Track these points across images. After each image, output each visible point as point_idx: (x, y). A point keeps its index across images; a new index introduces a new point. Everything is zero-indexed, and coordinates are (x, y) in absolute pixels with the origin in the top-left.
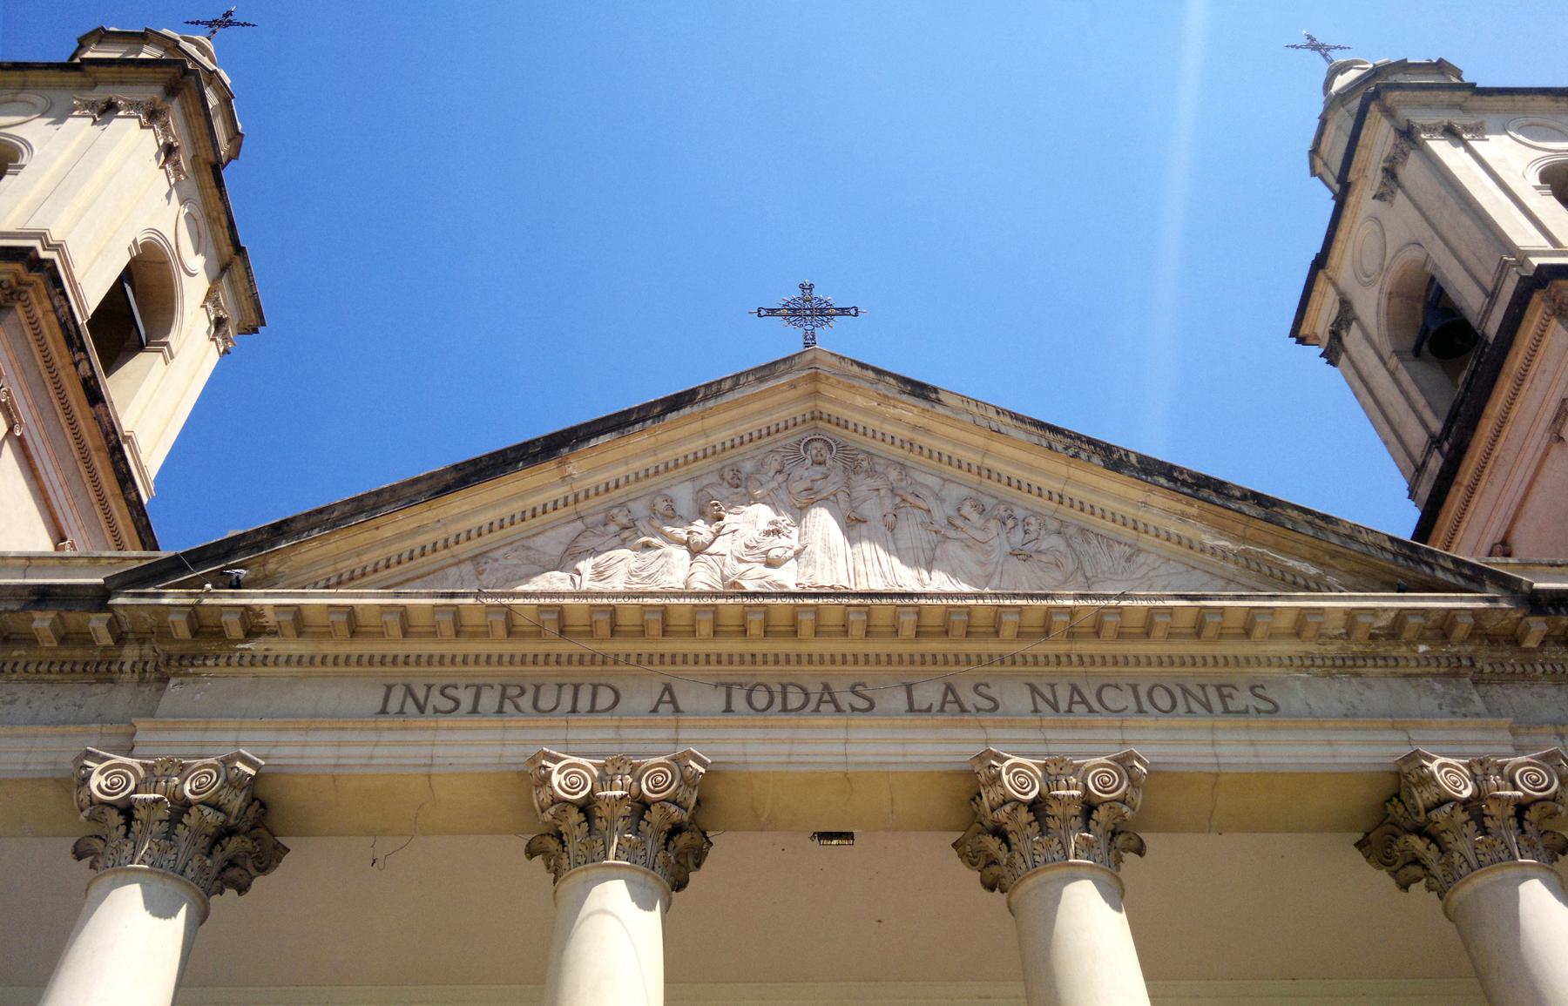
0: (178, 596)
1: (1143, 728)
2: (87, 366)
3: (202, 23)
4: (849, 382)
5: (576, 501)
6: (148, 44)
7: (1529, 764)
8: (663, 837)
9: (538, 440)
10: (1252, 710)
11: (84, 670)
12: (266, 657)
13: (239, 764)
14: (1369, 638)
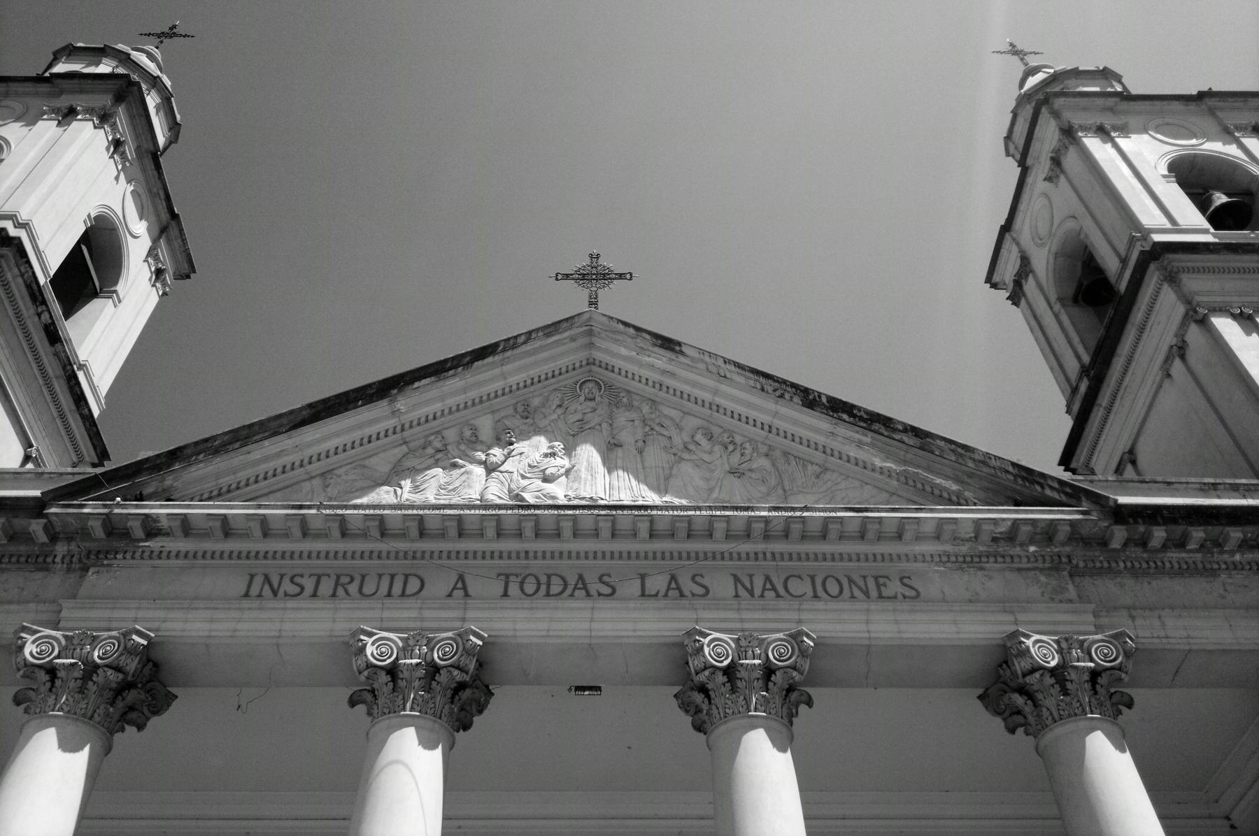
0: (95, 507)
1: (816, 610)
2: (48, 316)
3: (153, 35)
5: (403, 430)
6: (106, 57)
7: (1103, 641)
8: (449, 693)
9: (374, 383)
10: (900, 596)
11: (27, 561)
12: (161, 552)
13: (134, 637)
14: (992, 541)
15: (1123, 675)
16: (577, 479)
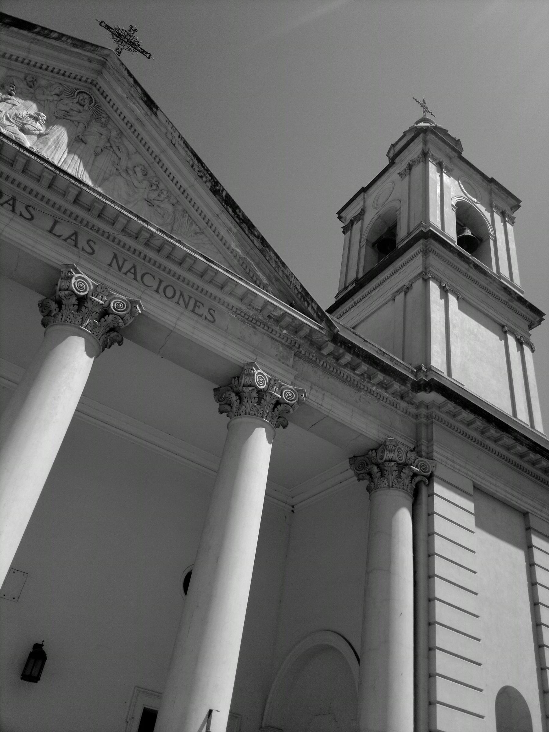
4: (119, 77)
10: (204, 317)
15: (291, 410)
16: (45, 143)
